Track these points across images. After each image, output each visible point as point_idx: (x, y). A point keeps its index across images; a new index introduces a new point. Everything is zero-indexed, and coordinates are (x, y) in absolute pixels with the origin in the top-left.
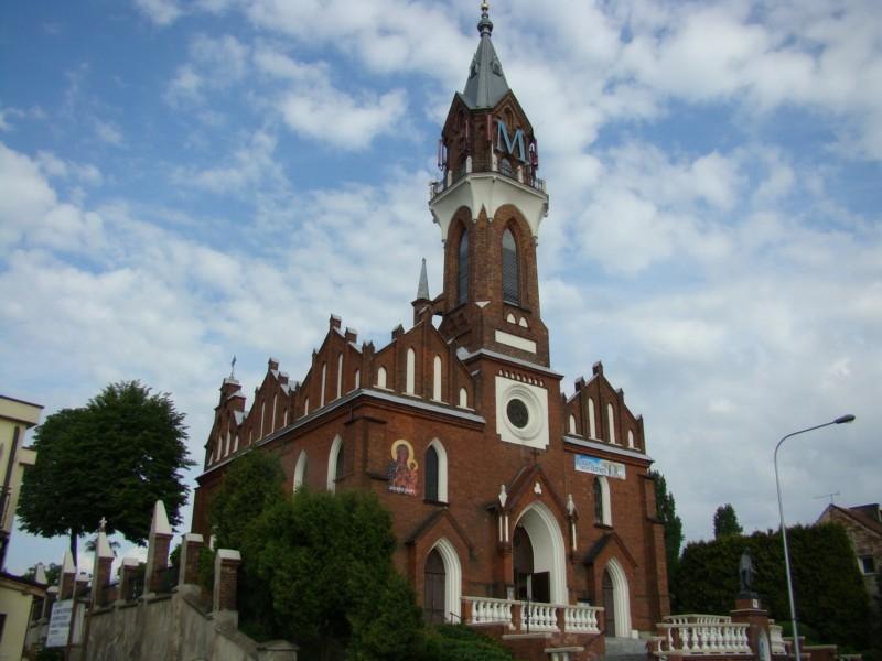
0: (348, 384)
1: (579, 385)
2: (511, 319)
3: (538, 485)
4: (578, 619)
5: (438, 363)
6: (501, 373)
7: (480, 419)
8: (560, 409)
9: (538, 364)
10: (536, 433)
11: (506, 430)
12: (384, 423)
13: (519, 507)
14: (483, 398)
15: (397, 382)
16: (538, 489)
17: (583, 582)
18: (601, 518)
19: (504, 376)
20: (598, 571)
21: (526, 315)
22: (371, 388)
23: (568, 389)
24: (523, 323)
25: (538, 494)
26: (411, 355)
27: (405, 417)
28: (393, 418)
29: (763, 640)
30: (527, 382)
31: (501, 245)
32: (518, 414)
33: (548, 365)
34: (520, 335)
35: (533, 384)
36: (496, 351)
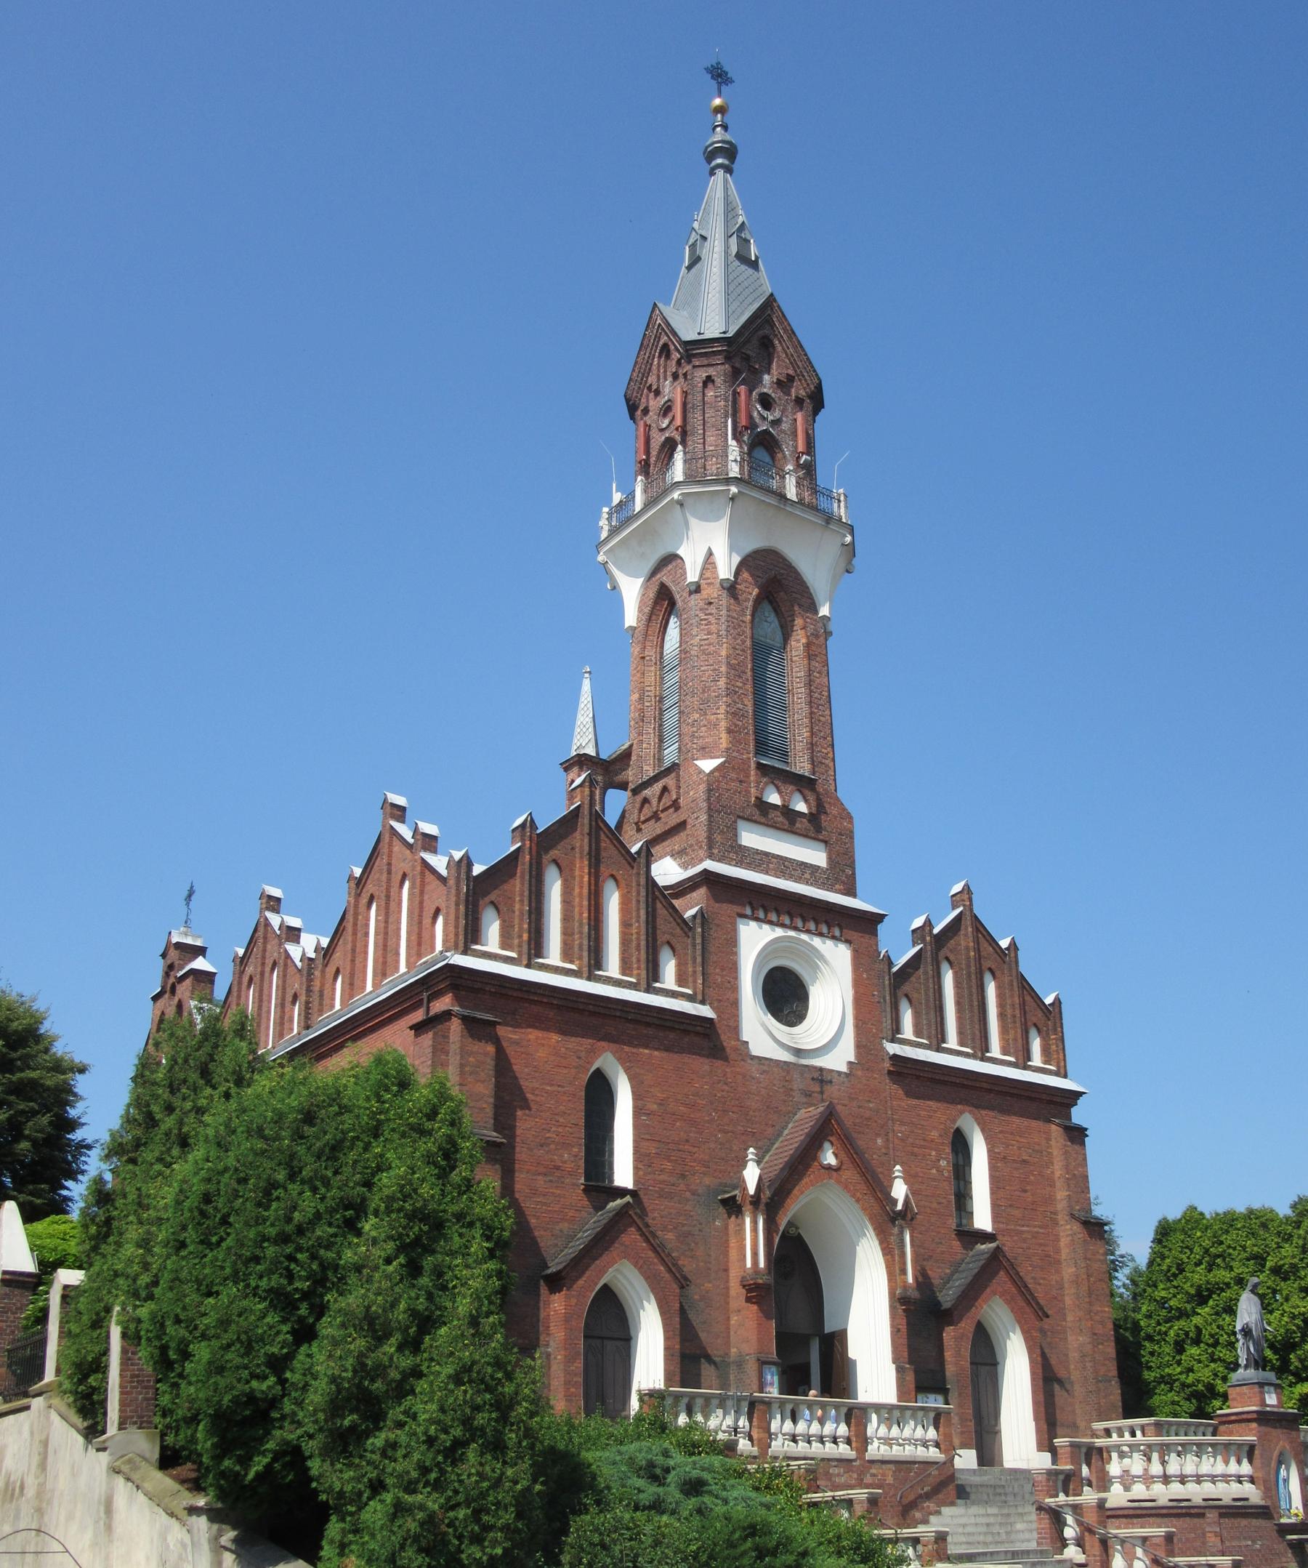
0: (420, 941)
4: (801, 1427)
7: (706, 1011)
8: (883, 990)
9: (831, 889)
11: (758, 1031)
14: (713, 971)
16: (829, 1158)
22: (466, 951)
25: (829, 1167)
32: (785, 994)
36: (739, 864)
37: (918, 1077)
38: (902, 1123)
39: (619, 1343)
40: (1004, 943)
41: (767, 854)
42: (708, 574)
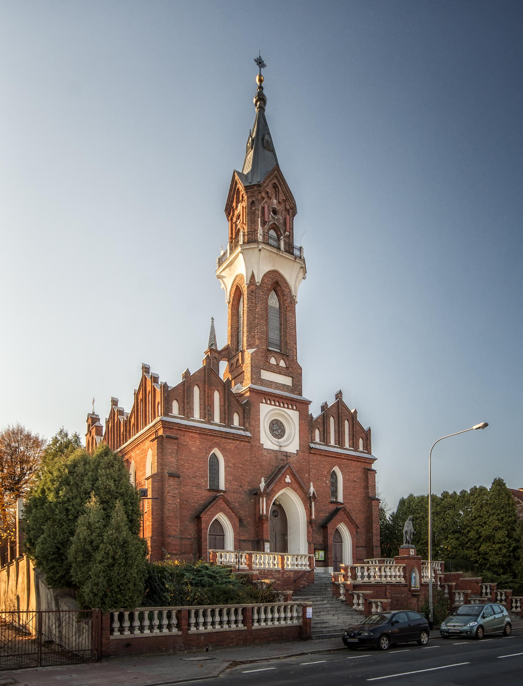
1: (324, 408)
2: (273, 361)
3: (288, 476)
5: (217, 395)
6: (264, 401)
7: (248, 434)
8: (308, 424)
10: (292, 444)
11: (268, 441)
12: (177, 439)
13: (274, 492)
15: (325, 439)
16: (288, 480)
17: (320, 539)
18: (336, 498)
19: (266, 403)
20: (330, 530)
21: (284, 357)
23: (315, 411)
24: (282, 364)
26: (196, 391)
27: (193, 434)
28: (184, 435)
29: (415, 575)
30: (284, 407)
31: (267, 304)
32: (277, 429)
33: (300, 394)
34: (280, 373)
35: (288, 408)
36: (261, 385)
37: (320, 455)
38: (314, 469)
39: (221, 537)
40: (352, 411)
41: (271, 382)
42: (252, 281)
